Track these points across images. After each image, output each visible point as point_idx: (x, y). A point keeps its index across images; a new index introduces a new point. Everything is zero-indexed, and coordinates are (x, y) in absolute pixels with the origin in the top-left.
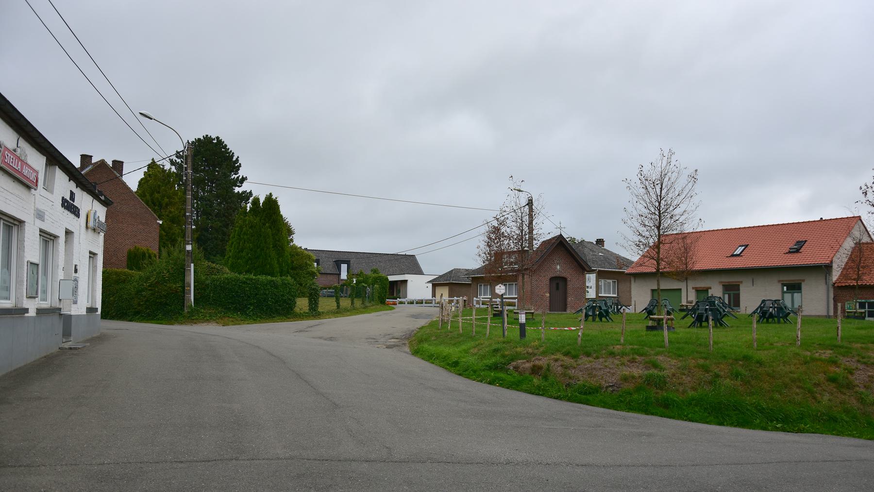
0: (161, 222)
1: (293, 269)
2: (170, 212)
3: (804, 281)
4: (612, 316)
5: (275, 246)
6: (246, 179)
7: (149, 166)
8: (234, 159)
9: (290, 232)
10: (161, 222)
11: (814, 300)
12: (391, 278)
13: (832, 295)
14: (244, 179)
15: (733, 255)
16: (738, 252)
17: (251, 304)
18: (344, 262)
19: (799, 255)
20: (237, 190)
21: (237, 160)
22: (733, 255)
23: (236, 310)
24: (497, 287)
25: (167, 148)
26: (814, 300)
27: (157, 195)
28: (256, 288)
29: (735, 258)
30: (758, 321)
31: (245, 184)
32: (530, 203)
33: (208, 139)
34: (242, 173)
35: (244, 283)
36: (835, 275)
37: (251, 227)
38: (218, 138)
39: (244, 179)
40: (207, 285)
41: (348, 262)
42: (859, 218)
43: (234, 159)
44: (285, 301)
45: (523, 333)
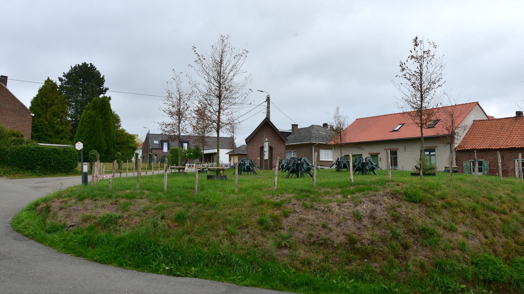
0: (33, 115)
1: (118, 144)
2: (53, 110)
3: (436, 147)
4: (257, 170)
5: (104, 129)
6: (108, 89)
7: (46, 82)
8: (101, 77)
9: (117, 120)
10: (33, 115)
11: (442, 159)
12: (206, 152)
13: (454, 157)
14: (107, 89)
15: (394, 131)
16: (397, 129)
17: (39, 165)
18: (165, 141)
19: (434, 129)
20: (101, 96)
21: (103, 78)
22: (394, 131)
23: (28, 169)
24: (77, 144)
25: (57, 71)
26: (442, 159)
27: (44, 99)
28: (43, 154)
29: (394, 133)
30: (354, 174)
31: (107, 92)
32: (268, 100)
33: (85, 65)
34: (105, 85)
35: (34, 150)
36: (457, 143)
37: (89, 118)
38: (91, 64)
39: (107, 89)
40: (7, 153)
41: (187, 142)
42: (477, 103)
43: (101, 77)
44: (66, 163)
45: (85, 181)
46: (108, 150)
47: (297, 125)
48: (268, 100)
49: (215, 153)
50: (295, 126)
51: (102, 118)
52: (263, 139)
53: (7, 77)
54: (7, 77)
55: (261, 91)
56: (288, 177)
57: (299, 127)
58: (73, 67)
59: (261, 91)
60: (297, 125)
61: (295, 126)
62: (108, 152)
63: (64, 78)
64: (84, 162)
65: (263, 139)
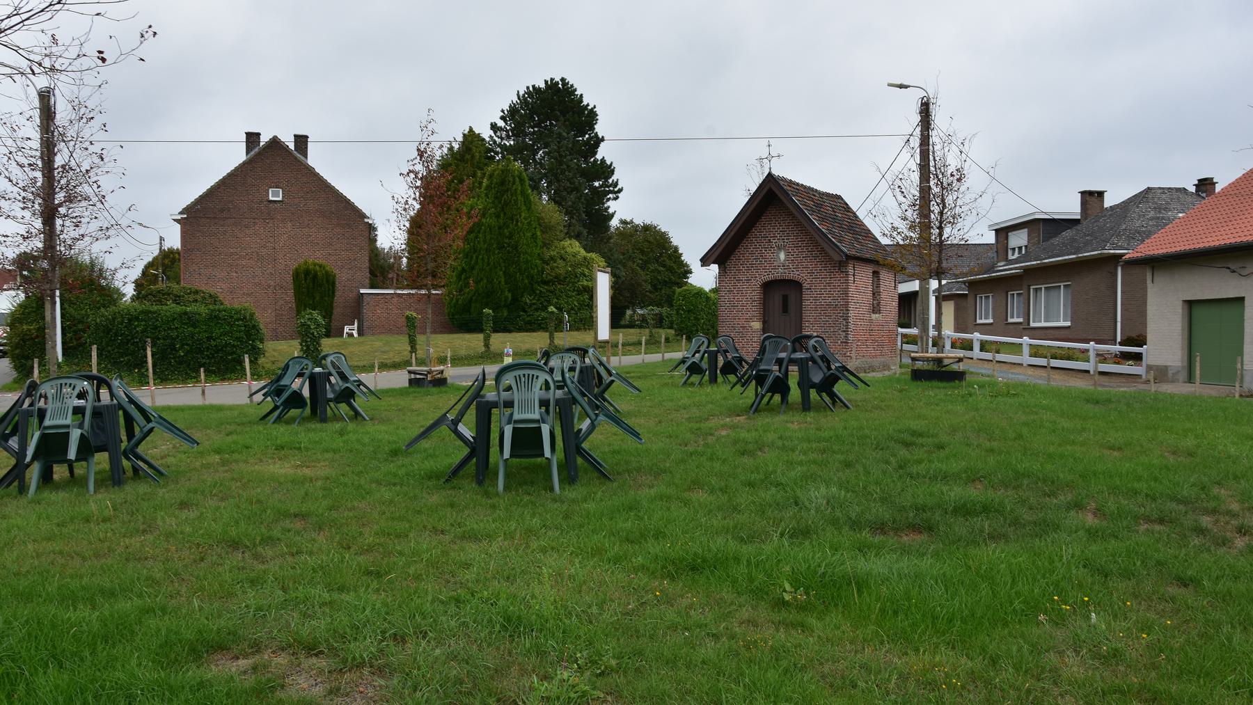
32: (925, 110)
35: (137, 319)
46: (515, 300)
47: (1101, 194)
48: (925, 110)
49: (915, 294)
50: (1091, 198)
51: (498, 217)
52: (769, 255)
53: (307, 137)
54: (307, 137)
55: (901, 86)
56: (756, 408)
57: (1109, 202)
58: (521, 93)
59: (901, 86)
60: (1101, 194)
61: (1091, 198)
62: (515, 304)
63: (501, 124)
64: (495, 331)
65: (769, 255)
